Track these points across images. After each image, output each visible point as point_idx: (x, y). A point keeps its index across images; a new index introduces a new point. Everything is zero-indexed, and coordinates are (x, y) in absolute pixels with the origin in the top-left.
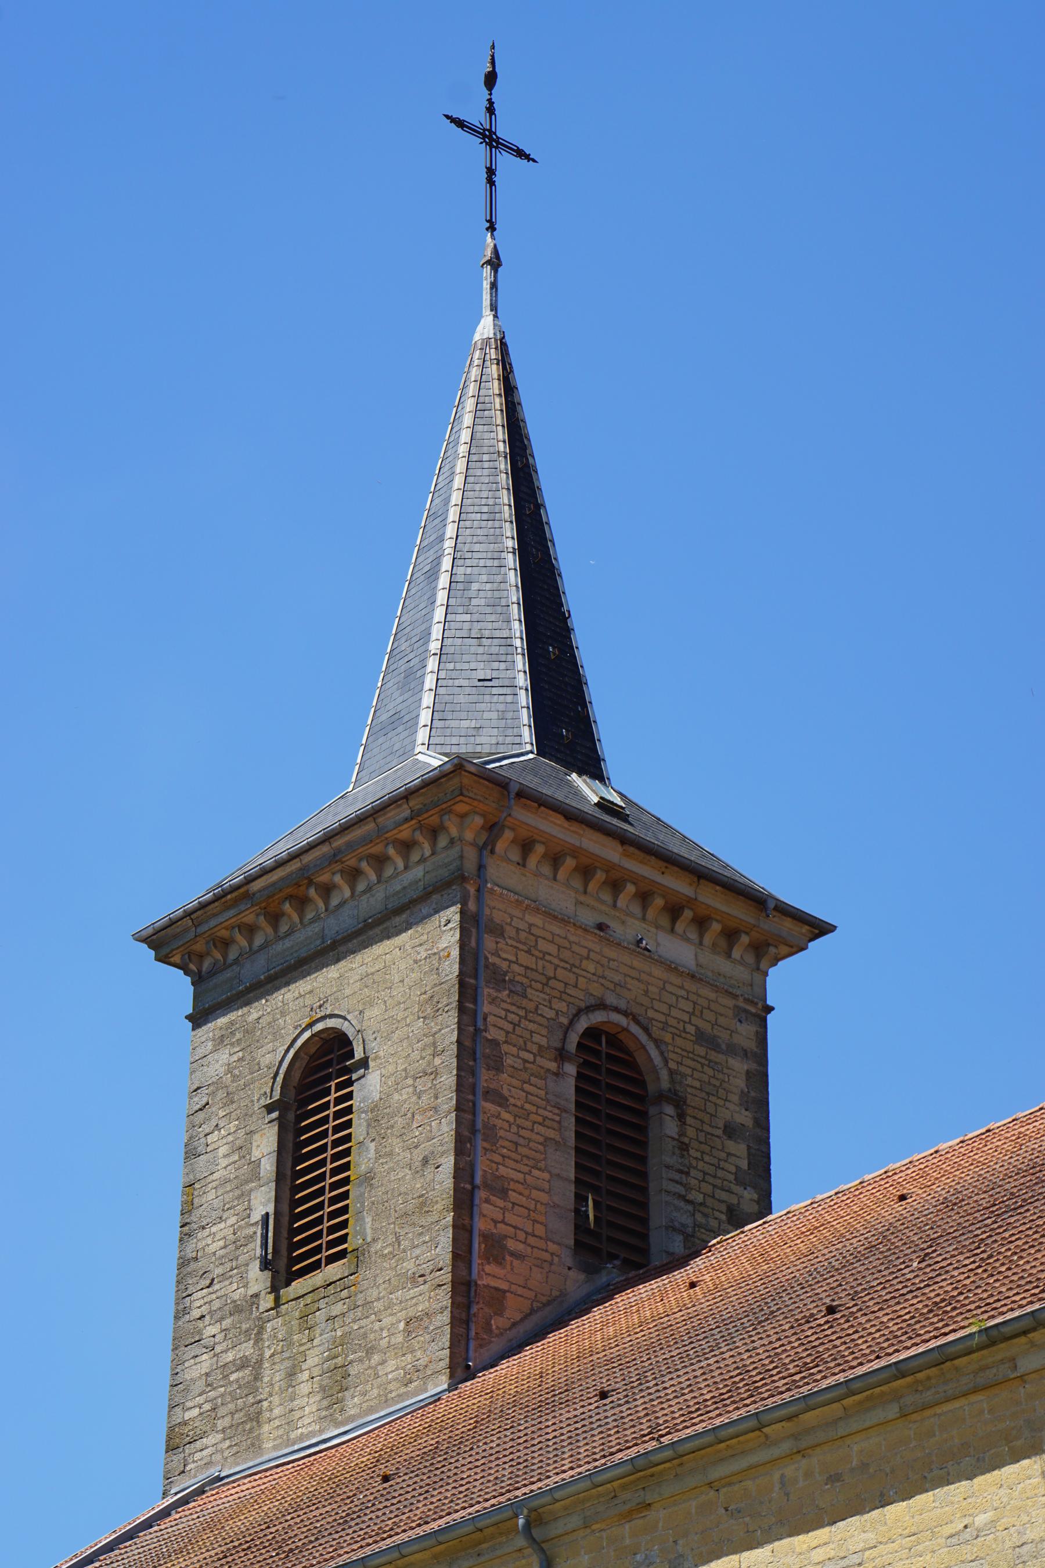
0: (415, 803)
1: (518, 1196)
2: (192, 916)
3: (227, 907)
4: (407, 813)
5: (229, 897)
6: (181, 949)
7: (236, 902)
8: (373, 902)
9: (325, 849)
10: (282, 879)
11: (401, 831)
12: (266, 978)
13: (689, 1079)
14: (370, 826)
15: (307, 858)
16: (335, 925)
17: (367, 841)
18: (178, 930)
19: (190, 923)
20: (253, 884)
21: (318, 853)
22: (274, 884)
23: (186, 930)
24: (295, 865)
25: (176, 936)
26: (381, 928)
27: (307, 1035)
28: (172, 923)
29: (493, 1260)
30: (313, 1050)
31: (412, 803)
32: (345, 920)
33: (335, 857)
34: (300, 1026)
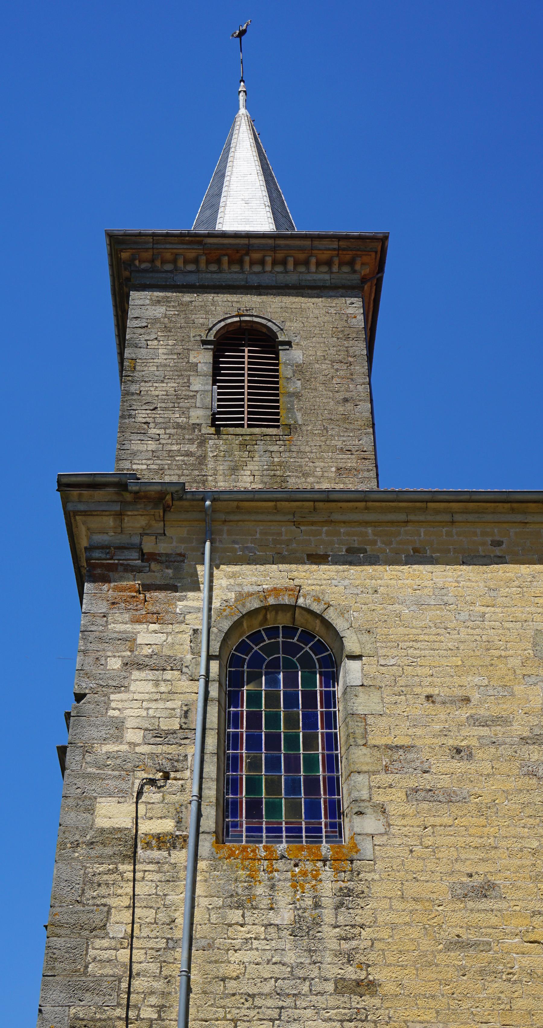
0: (343, 244)
1: (136, 789)
2: (155, 238)
3: (182, 243)
4: (336, 246)
5: (187, 238)
6: (134, 251)
7: (190, 243)
8: (292, 278)
9: (270, 241)
10: (230, 244)
11: (323, 254)
12: (199, 285)
13: (517, 627)
14: (308, 243)
15: (253, 241)
16: (254, 280)
17: (301, 249)
18: (140, 241)
19: (151, 240)
20: (209, 239)
21: (264, 242)
22: (223, 244)
23: (147, 243)
24: (245, 241)
25: (135, 243)
26: (296, 291)
27: (222, 324)
28: (140, 235)
29: (243, 595)
30: (231, 329)
31: (341, 243)
32: (266, 279)
33: (275, 249)
34: (230, 314)
